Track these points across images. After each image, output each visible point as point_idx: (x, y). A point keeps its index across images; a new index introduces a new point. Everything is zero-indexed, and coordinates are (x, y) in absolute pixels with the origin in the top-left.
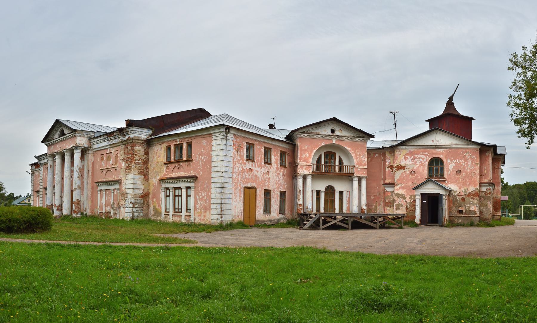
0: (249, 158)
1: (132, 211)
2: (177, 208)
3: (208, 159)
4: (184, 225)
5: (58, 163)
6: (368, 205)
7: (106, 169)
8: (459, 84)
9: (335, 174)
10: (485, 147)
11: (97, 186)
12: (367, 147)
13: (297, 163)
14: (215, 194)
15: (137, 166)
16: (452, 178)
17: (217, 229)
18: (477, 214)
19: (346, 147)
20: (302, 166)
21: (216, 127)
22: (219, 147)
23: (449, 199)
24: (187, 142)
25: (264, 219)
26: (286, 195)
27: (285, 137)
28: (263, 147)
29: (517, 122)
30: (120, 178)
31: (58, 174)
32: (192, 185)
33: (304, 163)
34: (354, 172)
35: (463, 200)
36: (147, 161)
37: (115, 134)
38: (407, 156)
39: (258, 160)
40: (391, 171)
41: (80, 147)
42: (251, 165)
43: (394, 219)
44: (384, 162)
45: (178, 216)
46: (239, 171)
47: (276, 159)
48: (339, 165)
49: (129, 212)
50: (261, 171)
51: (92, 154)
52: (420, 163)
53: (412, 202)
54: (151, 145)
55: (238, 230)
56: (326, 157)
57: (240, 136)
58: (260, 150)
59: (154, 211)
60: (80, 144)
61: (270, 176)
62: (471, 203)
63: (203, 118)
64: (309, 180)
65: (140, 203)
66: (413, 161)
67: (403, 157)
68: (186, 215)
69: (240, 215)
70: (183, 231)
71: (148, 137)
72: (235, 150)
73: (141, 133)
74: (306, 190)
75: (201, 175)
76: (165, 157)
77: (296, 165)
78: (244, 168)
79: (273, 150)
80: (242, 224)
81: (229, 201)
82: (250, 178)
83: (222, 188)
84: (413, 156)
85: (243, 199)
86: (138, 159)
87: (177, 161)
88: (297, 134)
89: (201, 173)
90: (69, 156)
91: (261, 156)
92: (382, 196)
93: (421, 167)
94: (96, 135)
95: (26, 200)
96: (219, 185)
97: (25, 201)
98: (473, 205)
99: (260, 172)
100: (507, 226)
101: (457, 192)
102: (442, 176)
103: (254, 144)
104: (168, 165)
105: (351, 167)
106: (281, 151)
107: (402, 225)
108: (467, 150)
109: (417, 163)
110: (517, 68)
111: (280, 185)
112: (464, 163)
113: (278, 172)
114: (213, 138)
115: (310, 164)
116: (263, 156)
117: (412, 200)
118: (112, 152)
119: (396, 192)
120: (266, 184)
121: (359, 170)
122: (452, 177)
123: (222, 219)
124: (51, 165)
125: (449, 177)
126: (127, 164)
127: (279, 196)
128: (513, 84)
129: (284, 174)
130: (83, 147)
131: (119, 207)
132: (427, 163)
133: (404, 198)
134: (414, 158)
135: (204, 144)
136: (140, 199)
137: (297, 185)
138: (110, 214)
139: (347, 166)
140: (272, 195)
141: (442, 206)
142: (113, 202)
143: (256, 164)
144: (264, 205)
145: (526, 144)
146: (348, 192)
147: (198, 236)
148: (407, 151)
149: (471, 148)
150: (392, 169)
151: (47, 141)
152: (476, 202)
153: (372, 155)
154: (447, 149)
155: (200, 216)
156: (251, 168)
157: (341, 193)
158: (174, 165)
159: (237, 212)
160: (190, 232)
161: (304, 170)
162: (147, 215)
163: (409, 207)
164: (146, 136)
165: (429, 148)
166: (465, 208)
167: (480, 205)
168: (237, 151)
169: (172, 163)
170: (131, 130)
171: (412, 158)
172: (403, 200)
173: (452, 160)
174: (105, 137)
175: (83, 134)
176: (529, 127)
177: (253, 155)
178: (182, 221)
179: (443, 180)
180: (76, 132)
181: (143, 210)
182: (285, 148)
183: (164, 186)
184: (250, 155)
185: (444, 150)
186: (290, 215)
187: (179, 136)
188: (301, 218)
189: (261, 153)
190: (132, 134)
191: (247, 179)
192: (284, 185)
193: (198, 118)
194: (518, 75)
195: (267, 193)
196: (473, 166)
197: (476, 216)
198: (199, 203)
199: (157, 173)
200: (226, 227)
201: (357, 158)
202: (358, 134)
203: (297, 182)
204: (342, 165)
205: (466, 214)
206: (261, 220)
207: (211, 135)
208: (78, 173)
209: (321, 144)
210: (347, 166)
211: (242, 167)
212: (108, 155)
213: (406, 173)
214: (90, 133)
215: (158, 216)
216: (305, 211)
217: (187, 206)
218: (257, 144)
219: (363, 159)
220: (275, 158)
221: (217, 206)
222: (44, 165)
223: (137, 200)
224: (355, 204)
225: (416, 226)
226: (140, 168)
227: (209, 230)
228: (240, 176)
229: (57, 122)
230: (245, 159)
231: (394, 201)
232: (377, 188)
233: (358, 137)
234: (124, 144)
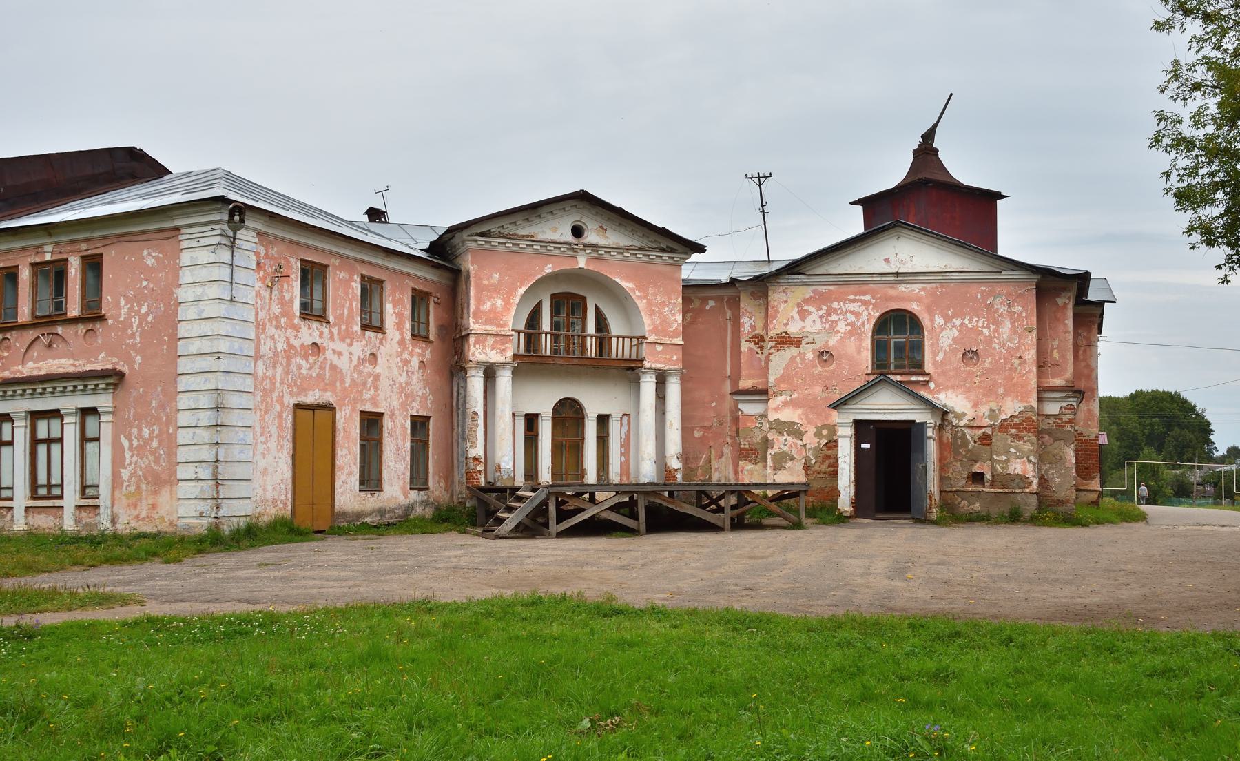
0: (311, 312)
2: (45, 482)
3: (164, 312)
4: (75, 540)
6: (685, 457)
8: (951, 94)
9: (586, 362)
10: (1057, 279)
12: (683, 280)
13: (467, 329)
16: (951, 373)
17: (200, 547)
18: (1030, 484)
19: (618, 280)
21: (195, 205)
22: (203, 274)
23: (940, 438)
25: (362, 508)
27: (427, 245)
28: (355, 277)
29: (1184, 197)
32: (102, 401)
33: (489, 328)
34: (644, 355)
35: (985, 440)
38: (806, 307)
39: (340, 318)
40: (757, 353)
42: (317, 333)
43: (777, 499)
44: (733, 326)
45: (48, 509)
46: (276, 353)
47: (400, 315)
48: (598, 335)
50: (351, 354)
52: (849, 328)
53: (824, 448)
55: (278, 546)
56: (555, 310)
57: (281, 239)
58: (346, 283)
61: (378, 370)
62: (1012, 450)
63: (141, 178)
64: (504, 380)
66: (827, 321)
67: (796, 309)
68: (79, 507)
69: (283, 497)
70: (74, 564)
72: (264, 283)
74: (494, 414)
75: (137, 367)
77: (463, 334)
78: (292, 341)
79: (388, 287)
80: (290, 528)
81: (241, 452)
82: (314, 375)
83: (217, 408)
84: (824, 307)
85: (290, 445)
87: (39, 322)
88: (465, 237)
91: (351, 305)
92: (728, 429)
93: (852, 338)
96: (205, 401)
98: (1018, 457)
99: (346, 355)
100: (1126, 525)
101: (967, 418)
102: (919, 367)
103: (326, 266)
104: (8, 336)
105: (634, 342)
106: (414, 290)
107: (800, 519)
108: (998, 288)
109: (838, 328)
110: (1189, 19)
111: (410, 396)
112: (988, 327)
113: (406, 356)
114: (182, 243)
115: (507, 330)
116: (357, 304)
117: (824, 441)
119: (772, 416)
120: (367, 396)
121: (659, 348)
122: (950, 371)
123: (220, 514)
125: (939, 370)
127: (409, 431)
128: (1169, 76)
129: (422, 362)
132: (869, 328)
133: (798, 434)
134: (829, 314)
135: (150, 262)
137: (465, 396)
139: (623, 338)
140: (385, 429)
141: (923, 458)
143: (335, 331)
144: (360, 463)
145: (1219, 267)
146: (625, 418)
147: (137, 577)
148: (807, 292)
149: (1007, 281)
150: (759, 347)
152: (1027, 447)
153: (696, 304)
154: (934, 285)
155: (135, 506)
156: (319, 341)
157: (603, 420)
158: (31, 334)
159: (270, 488)
160: (102, 563)
161: (488, 351)
163: (813, 462)
165: (874, 283)
166: (993, 468)
167: (1041, 459)
168: (271, 288)
169: (24, 327)
171: (821, 313)
172: (795, 440)
173: (948, 319)
176: (1227, 213)
177: (324, 301)
178: (65, 527)
179: (921, 378)
182: (427, 280)
184: (312, 300)
185: (923, 289)
186: (444, 493)
187: (50, 235)
188: (479, 500)
189: (350, 296)
191: (303, 378)
192: (424, 397)
193: (122, 178)
194: (1194, 44)
195: (371, 423)
196: (1016, 337)
197: (1027, 490)
200: (232, 539)
201: (652, 314)
202: (655, 241)
203: (465, 388)
204: (606, 335)
205: (996, 484)
206: (353, 512)
207: (174, 233)
210: (621, 337)
211: (288, 339)
213: (803, 359)
216: (491, 479)
217: (83, 475)
218: (336, 268)
219: (670, 316)
220: (396, 311)
221: (198, 470)
224: (645, 456)
225: (841, 519)
227: (173, 554)
228: (279, 370)
230: (298, 314)
231: (767, 443)
232: (714, 404)
233: (654, 250)
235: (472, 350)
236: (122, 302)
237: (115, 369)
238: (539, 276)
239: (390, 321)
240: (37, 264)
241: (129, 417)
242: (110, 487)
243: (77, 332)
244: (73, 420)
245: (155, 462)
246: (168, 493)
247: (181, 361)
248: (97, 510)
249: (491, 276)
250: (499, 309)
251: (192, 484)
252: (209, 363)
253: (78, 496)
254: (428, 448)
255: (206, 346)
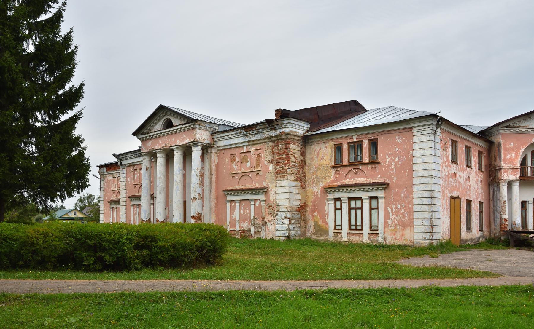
1: (289, 228)
2: (355, 224)
3: (406, 160)
4: (369, 246)
5: (161, 164)
7: (241, 174)
11: (225, 196)
14: (421, 205)
15: (293, 169)
20: (506, 169)
22: (424, 145)
24: (370, 138)
26: (483, 206)
30: (265, 185)
31: (161, 178)
32: (380, 194)
33: (509, 165)
36: (303, 164)
37: (257, 128)
41: (201, 143)
47: (475, 161)
49: (283, 230)
51: (216, 153)
54: (309, 143)
59: (314, 228)
60: (201, 139)
61: (470, 183)
64: (516, 187)
65: (297, 218)
71: (305, 133)
73: (298, 127)
75: (394, 181)
76: (333, 159)
83: (432, 197)
86: (294, 161)
87: (350, 164)
89: (395, 178)
90: (180, 154)
94: (221, 129)
95: (70, 213)
97: (69, 213)
104: (339, 169)
106: (479, 151)
113: (477, 178)
118: (250, 152)
123: (433, 239)
124: (147, 167)
126: (279, 167)
130: (205, 143)
131: (265, 224)
135: (399, 141)
136: (297, 213)
138: (248, 233)
142: (254, 217)
151: (142, 134)
155: (394, 234)
158: (348, 169)
159: (444, 229)
161: (509, 175)
162: (304, 233)
164: (303, 132)
169: (345, 166)
170: (287, 122)
174: (239, 131)
175: (205, 127)
180: (196, 123)
181: (300, 227)
183: (331, 196)
187: (356, 132)
190: (288, 127)
191: (452, 186)
195: (469, 202)
198: (392, 218)
199: (319, 179)
207: (411, 129)
208: (198, 178)
209: (531, 140)
212: (244, 154)
214: (214, 125)
215: (321, 235)
222: (128, 166)
223: (294, 214)
226: (296, 172)
229: (161, 108)
234: (272, 141)
235: (503, 175)
236: (387, 157)
237: (385, 182)
238: (530, 143)
239: (473, 164)
240: (350, 143)
241: (391, 200)
242: (384, 227)
243: (368, 168)
244: (367, 201)
245: (403, 218)
246: (409, 230)
247: (414, 179)
248: (378, 235)
249: (510, 144)
250: (514, 157)
251: (421, 226)
252: (428, 180)
253: (369, 229)
254: (482, 214)
255: (426, 173)
